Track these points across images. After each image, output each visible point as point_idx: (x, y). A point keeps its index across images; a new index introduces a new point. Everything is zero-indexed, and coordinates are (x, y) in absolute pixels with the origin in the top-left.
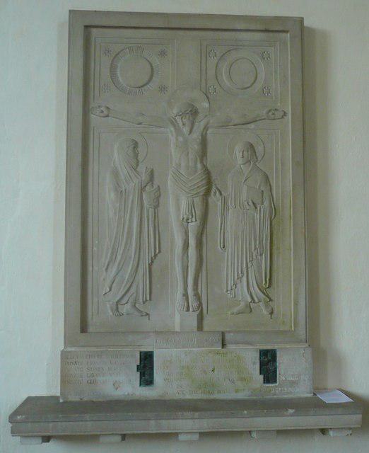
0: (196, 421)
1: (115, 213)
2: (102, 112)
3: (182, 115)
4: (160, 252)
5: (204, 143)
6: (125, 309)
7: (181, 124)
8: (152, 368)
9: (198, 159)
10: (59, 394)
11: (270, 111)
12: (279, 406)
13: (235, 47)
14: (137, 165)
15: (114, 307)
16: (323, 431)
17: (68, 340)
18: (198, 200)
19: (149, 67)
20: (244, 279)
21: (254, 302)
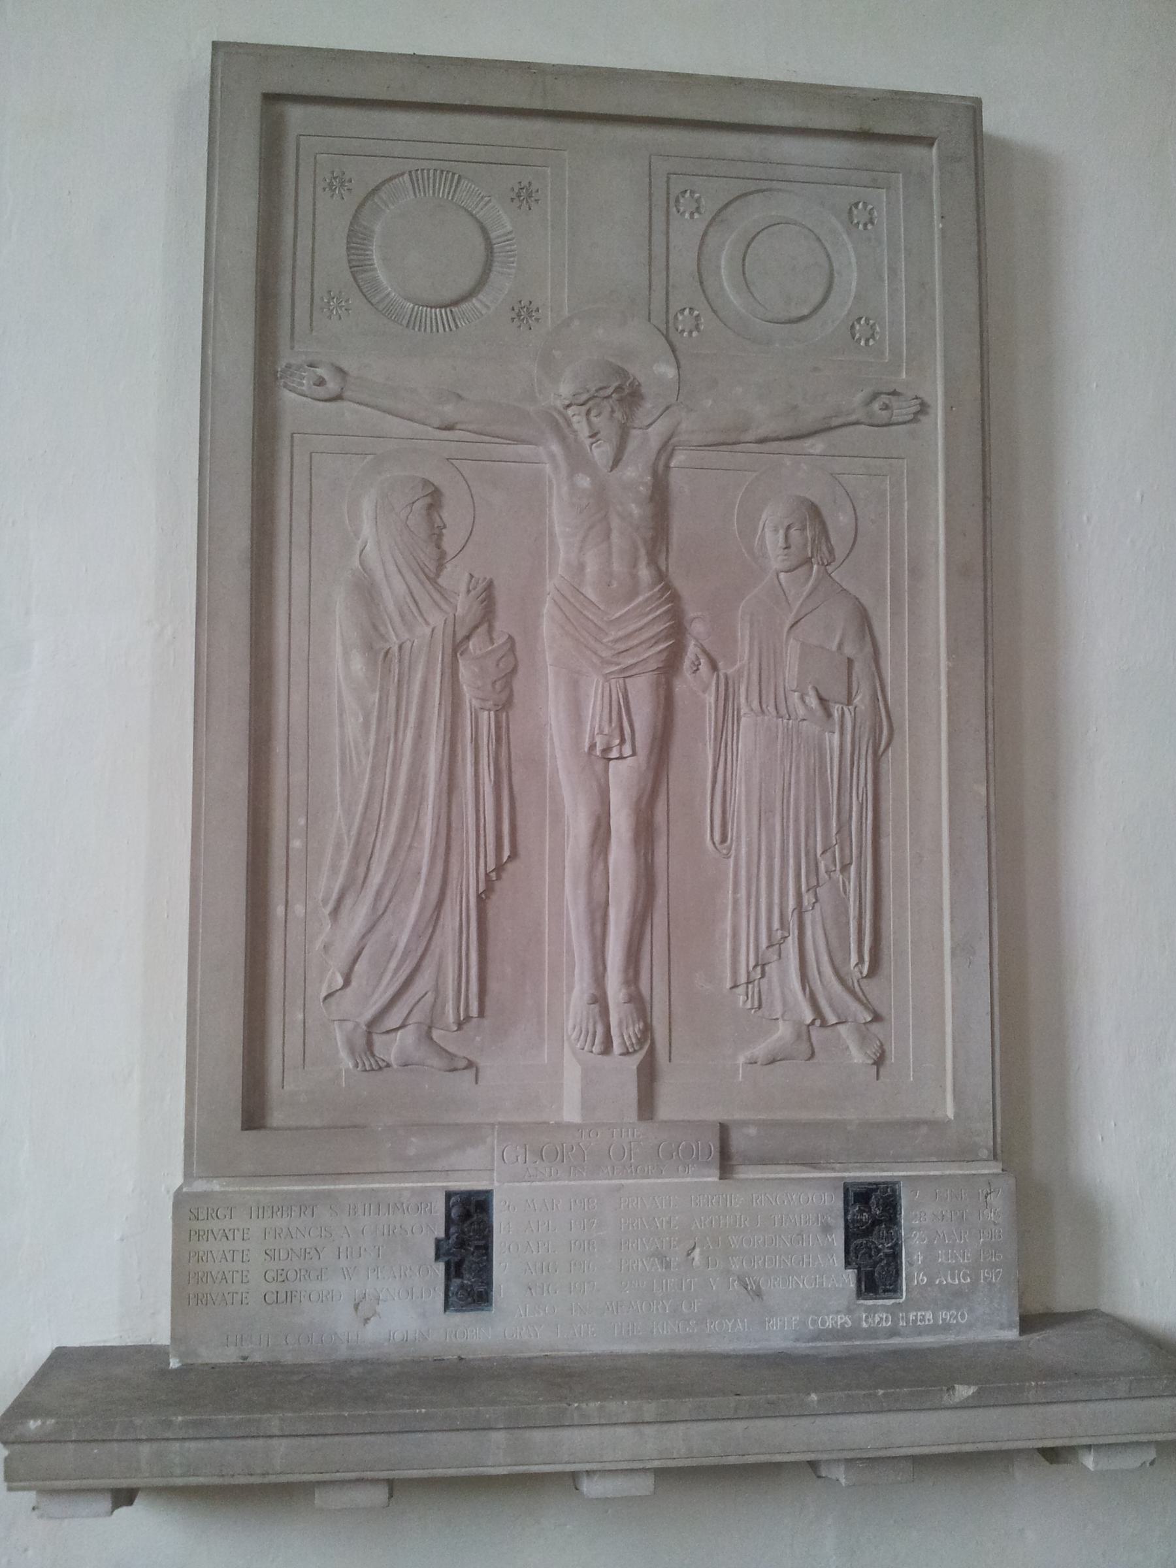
0: (649, 1430)
1: (366, 725)
2: (321, 382)
3: (588, 402)
4: (514, 855)
5: (660, 497)
6: (394, 1051)
7: (584, 432)
8: (486, 1249)
9: (642, 552)
10: (163, 1338)
11: (875, 396)
12: (910, 1375)
13: (764, 185)
14: (440, 567)
15: (361, 1042)
16: (1052, 1455)
17: (200, 1154)
18: (641, 692)
19: (479, 241)
20: (791, 946)
21: (824, 1024)
